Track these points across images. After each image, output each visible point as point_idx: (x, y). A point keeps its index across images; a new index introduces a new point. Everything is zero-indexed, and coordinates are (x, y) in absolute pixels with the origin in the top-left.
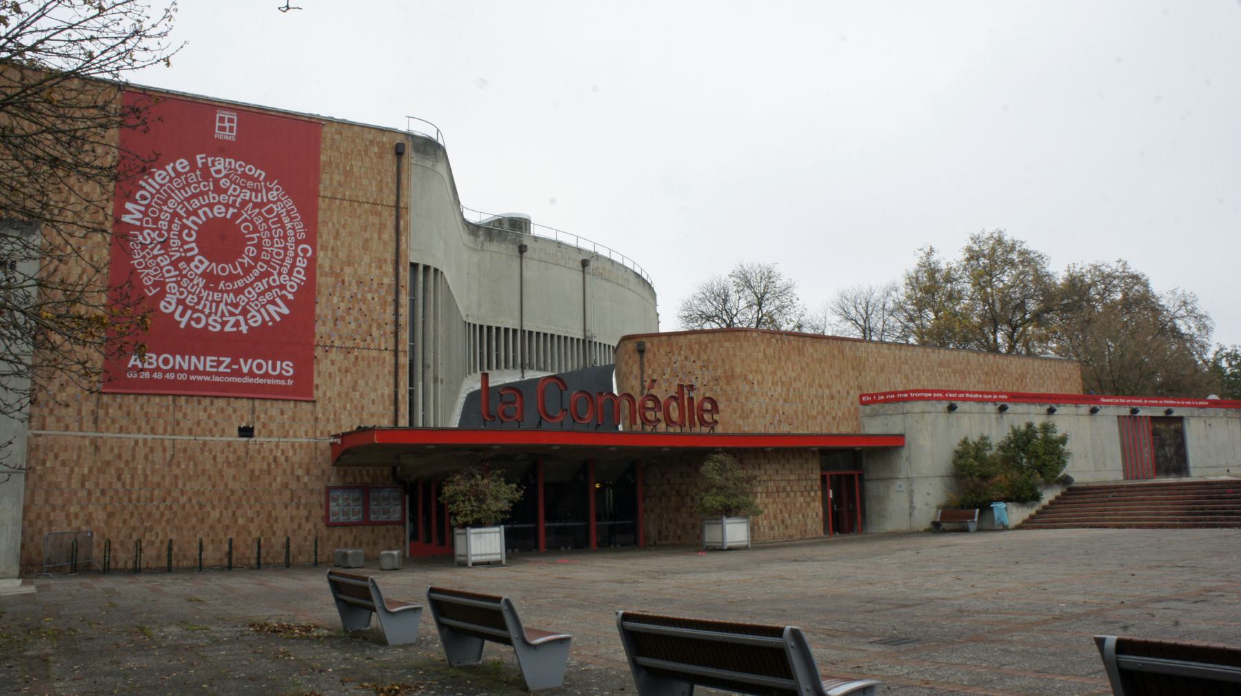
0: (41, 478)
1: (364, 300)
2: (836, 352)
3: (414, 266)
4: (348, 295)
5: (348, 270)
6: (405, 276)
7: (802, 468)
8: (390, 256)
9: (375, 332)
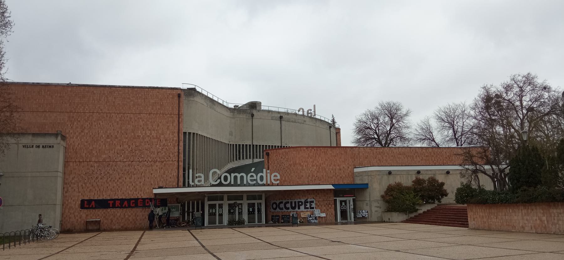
0: (67, 205)
1: (167, 146)
2: (343, 152)
3: (185, 133)
4: (162, 144)
5: (162, 136)
6: (182, 137)
7: (325, 196)
8: (176, 131)
9: (171, 156)
